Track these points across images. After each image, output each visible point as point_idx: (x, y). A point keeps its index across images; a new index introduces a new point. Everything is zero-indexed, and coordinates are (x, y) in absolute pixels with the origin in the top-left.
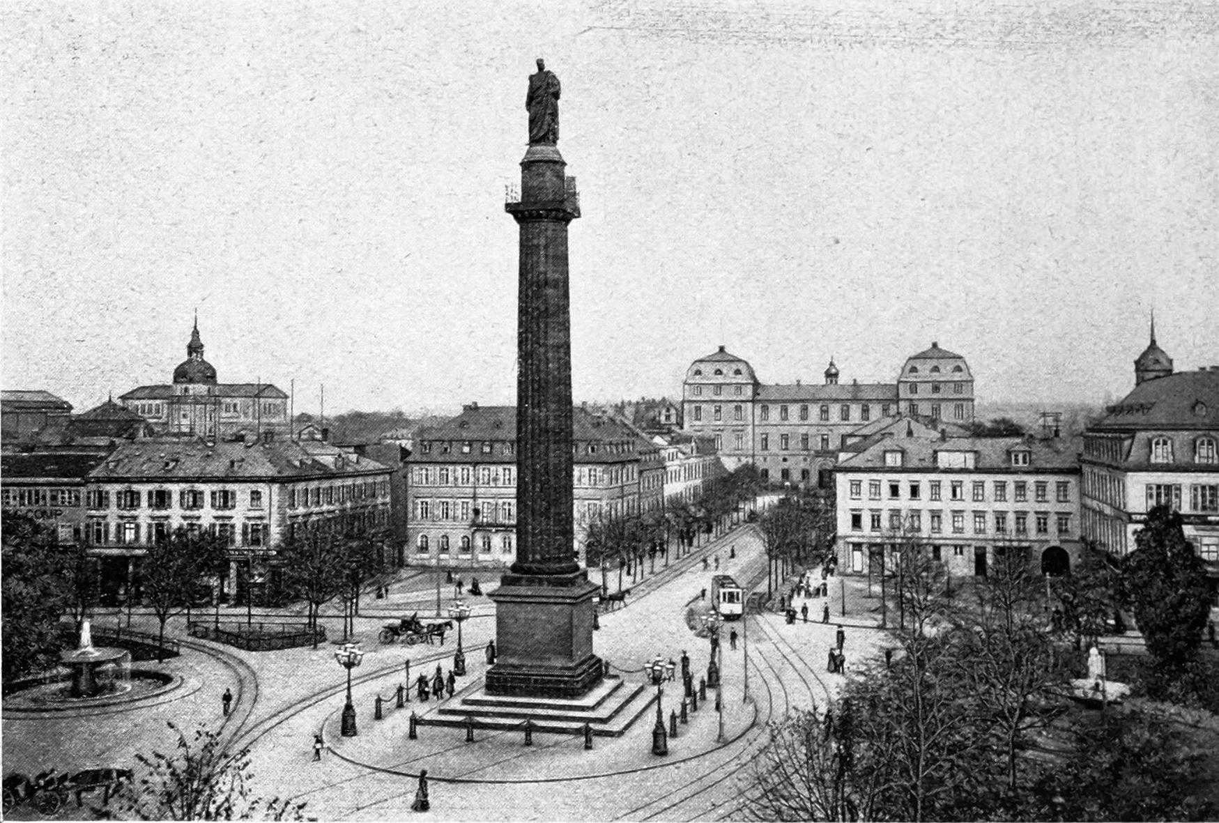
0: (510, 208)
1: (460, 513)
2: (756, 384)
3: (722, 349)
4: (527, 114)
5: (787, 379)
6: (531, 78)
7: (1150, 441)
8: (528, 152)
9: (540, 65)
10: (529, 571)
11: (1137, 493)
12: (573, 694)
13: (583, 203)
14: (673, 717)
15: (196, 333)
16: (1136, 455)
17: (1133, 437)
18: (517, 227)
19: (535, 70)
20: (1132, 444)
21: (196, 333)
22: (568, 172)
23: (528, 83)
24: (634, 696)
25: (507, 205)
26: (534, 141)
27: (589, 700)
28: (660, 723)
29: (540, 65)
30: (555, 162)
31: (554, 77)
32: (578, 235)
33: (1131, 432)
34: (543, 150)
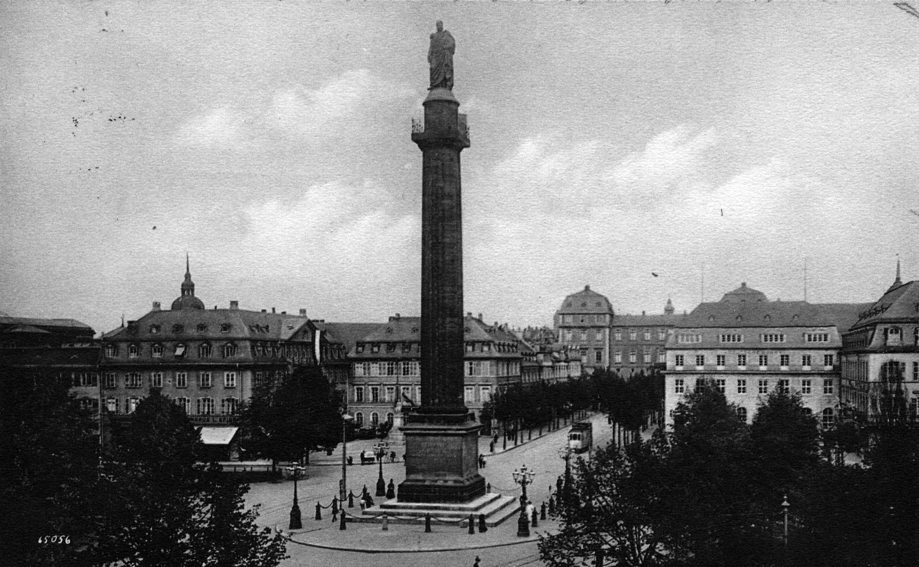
0: (416, 138)
1: (385, 391)
2: (612, 315)
3: (587, 288)
4: (428, 65)
5: (636, 311)
6: (432, 37)
7: (886, 330)
8: (430, 94)
9: (439, 25)
10: (430, 411)
11: (875, 363)
12: (463, 501)
13: (473, 136)
14: (535, 513)
15: (188, 276)
16: (876, 341)
17: (874, 330)
18: (421, 153)
19: (434, 30)
20: (873, 334)
21: (188, 276)
22: (461, 110)
23: (429, 40)
24: (507, 504)
25: (413, 135)
26: (433, 87)
27: (473, 505)
28: (524, 515)
29: (439, 25)
30: (450, 102)
31: (450, 35)
32: (469, 160)
33: (874, 325)
34: (440, 93)
